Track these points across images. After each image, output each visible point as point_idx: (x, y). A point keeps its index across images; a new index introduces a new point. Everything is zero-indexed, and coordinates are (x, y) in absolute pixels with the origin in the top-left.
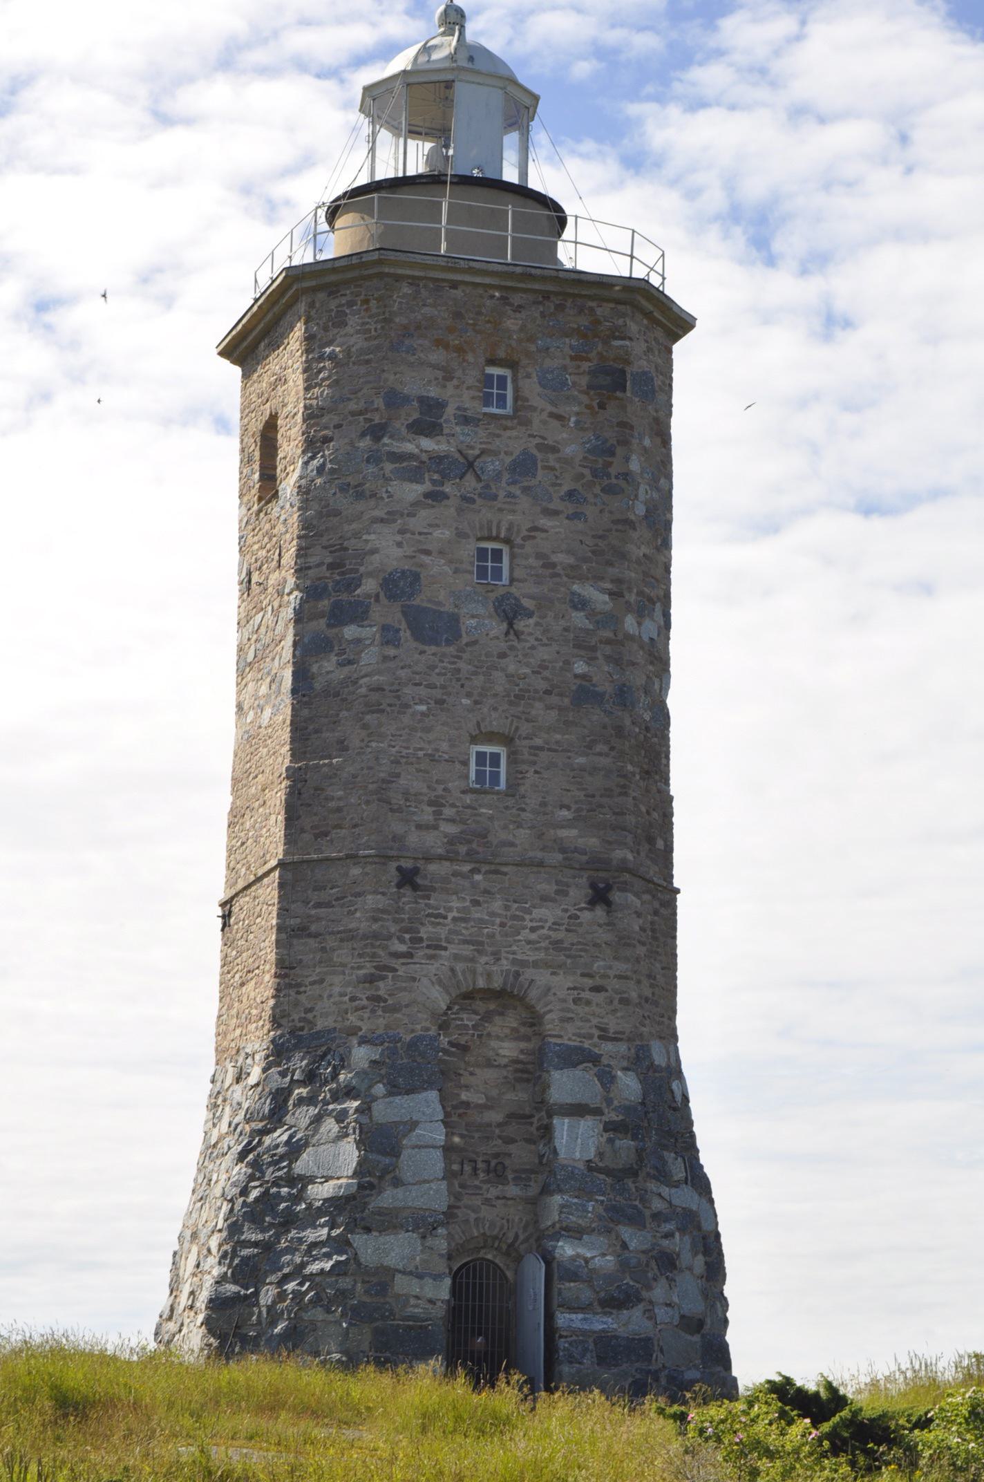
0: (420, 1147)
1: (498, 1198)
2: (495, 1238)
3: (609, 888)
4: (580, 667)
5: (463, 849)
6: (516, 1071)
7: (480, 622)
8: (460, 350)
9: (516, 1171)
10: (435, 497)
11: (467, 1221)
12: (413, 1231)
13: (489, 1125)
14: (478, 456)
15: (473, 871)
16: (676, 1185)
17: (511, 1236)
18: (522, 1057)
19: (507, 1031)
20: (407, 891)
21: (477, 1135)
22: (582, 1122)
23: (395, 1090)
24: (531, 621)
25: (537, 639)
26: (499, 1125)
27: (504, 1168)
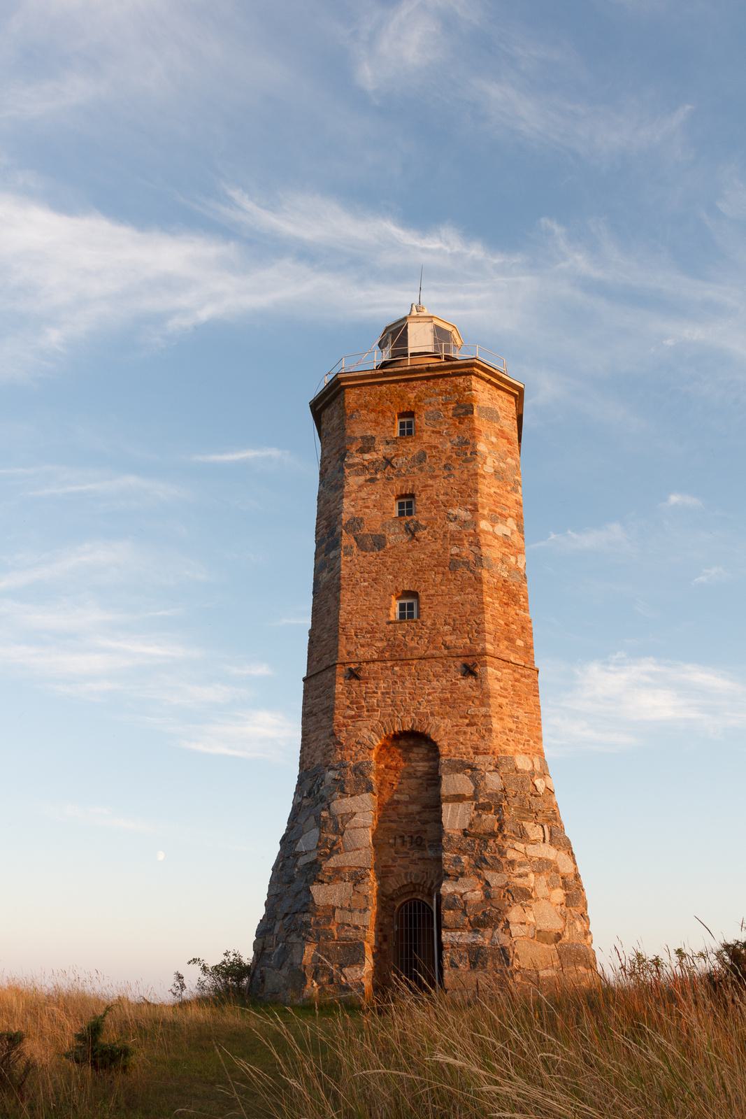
0: (355, 828)
1: (419, 859)
2: (419, 884)
3: (475, 665)
4: (454, 550)
5: (387, 655)
6: (428, 779)
7: (396, 537)
8: (383, 412)
9: (429, 841)
10: (372, 480)
11: (400, 875)
12: (349, 881)
13: (412, 814)
14: (393, 458)
15: (393, 666)
16: (534, 842)
17: (429, 883)
18: (431, 770)
19: (421, 756)
20: (355, 683)
21: (404, 821)
22: (461, 805)
23: (344, 795)
24: (425, 532)
25: (429, 540)
26: (419, 813)
27: (422, 840)
